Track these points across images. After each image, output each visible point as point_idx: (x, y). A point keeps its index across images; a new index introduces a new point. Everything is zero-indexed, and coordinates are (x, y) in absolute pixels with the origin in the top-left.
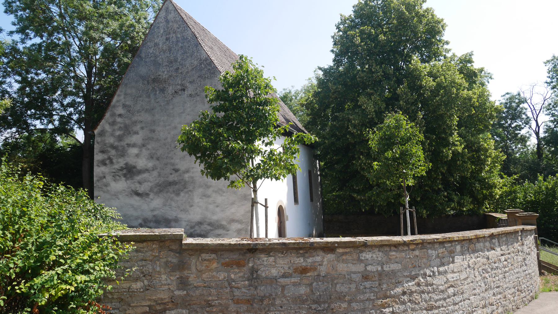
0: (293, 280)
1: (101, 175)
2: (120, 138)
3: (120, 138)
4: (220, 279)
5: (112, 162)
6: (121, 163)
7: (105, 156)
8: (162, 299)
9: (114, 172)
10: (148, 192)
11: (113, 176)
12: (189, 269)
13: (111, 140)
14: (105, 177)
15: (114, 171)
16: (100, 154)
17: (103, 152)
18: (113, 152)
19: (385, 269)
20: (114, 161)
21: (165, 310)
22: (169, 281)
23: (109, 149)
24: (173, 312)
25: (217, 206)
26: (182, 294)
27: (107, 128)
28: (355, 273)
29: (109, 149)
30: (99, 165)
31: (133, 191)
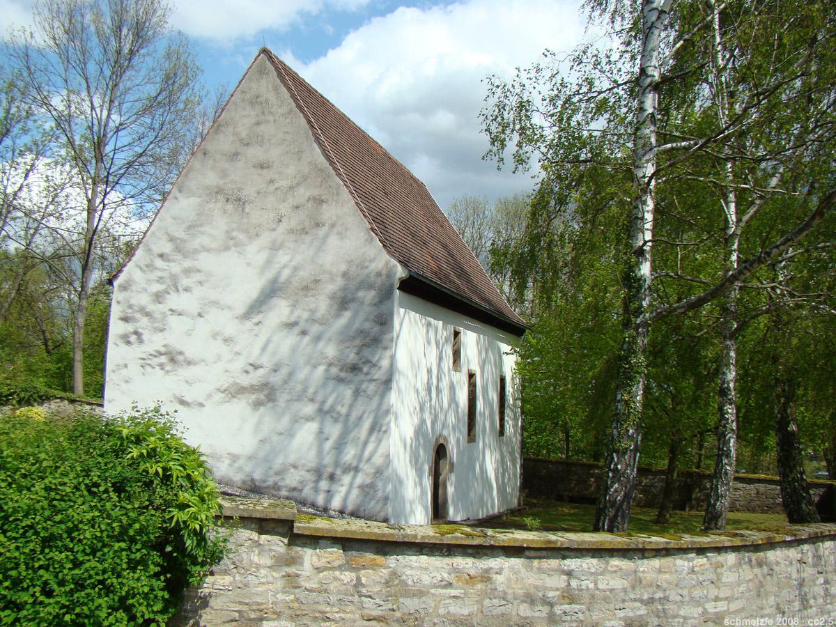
0: (453, 592)
1: (122, 362)
2: (158, 298)
3: (158, 298)
4: (345, 582)
5: (140, 341)
6: (155, 341)
7: (130, 328)
8: (259, 604)
9: (143, 359)
10: (202, 401)
11: (142, 366)
12: (301, 564)
13: (143, 300)
14: (126, 366)
15: (144, 357)
16: (121, 323)
17: (125, 319)
18: (144, 321)
19: (601, 586)
20: (145, 337)
21: (261, 619)
22: (270, 579)
23: (138, 316)
24: (271, 623)
25: (232, 239)
26: (287, 598)
27: (138, 276)
28: (551, 589)
29: (138, 316)
30: (118, 342)
31: (176, 398)
